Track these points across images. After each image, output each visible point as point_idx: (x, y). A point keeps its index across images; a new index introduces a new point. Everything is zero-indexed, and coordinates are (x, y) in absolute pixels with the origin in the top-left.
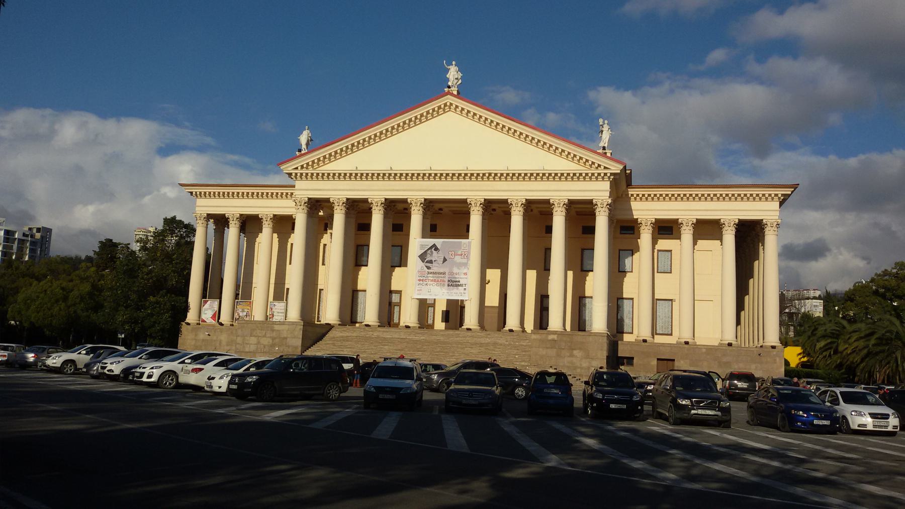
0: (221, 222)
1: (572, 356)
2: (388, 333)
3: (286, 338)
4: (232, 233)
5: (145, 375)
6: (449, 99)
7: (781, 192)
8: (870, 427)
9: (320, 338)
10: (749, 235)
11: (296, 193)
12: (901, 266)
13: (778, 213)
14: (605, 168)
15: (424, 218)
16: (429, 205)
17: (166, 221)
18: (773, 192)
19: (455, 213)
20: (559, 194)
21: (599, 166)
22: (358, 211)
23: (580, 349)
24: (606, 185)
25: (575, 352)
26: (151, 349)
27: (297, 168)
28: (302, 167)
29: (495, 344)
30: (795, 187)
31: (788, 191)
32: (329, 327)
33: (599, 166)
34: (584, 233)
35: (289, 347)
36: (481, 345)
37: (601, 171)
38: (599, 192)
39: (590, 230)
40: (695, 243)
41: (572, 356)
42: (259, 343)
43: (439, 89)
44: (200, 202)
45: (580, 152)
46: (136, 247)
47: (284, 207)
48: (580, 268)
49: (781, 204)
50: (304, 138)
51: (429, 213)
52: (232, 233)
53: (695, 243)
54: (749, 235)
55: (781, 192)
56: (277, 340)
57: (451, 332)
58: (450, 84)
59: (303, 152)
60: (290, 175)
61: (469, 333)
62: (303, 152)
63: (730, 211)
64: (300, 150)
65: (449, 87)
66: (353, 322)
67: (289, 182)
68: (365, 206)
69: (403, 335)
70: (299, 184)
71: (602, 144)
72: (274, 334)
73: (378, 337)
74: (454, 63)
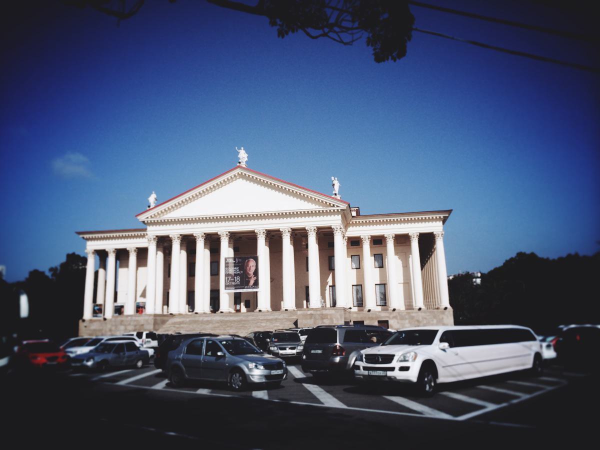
0: (102, 255)
2: (277, 315)
3: (143, 325)
5: (395, 364)
6: (238, 171)
10: (427, 242)
11: (148, 233)
13: (442, 228)
14: (337, 206)
17: (69, 256)
20: (311, 224)
21: (334, 205)
22: (189, 243)
23: (327, 318)
24: (339, 217)
26: (289, 347)
27: (148, 218)
29: (276, 319)
30: (450, 212)
33: (334, 205)
36: (268, 320)
37: (335, 208)
39: (331, 245)
40: (137, 269)
42: (126, 329)
43: (236, 165)
44: (89, 243)
45: (322, 198)
46: (48, 274)
47: (141, 243)
48: (328, 268)
49: (444, 222)
50: (152, 199)
51: (232, 240)
53: (137, 269)
54: (427, 242)
57: (249, 313)
58: (240, 161)
59: (151, 207)
60: (144, 222)
61: (260, 313)
62: (151, 207)
63: (414, 229)
64: (149, 207)
65: (240, 163)
67: (143, 226)
69: (286, 315)
70: (149, 228)
71: (334, 192)
72: (135, 323)
73: (202, 321)
74: (242, 148)
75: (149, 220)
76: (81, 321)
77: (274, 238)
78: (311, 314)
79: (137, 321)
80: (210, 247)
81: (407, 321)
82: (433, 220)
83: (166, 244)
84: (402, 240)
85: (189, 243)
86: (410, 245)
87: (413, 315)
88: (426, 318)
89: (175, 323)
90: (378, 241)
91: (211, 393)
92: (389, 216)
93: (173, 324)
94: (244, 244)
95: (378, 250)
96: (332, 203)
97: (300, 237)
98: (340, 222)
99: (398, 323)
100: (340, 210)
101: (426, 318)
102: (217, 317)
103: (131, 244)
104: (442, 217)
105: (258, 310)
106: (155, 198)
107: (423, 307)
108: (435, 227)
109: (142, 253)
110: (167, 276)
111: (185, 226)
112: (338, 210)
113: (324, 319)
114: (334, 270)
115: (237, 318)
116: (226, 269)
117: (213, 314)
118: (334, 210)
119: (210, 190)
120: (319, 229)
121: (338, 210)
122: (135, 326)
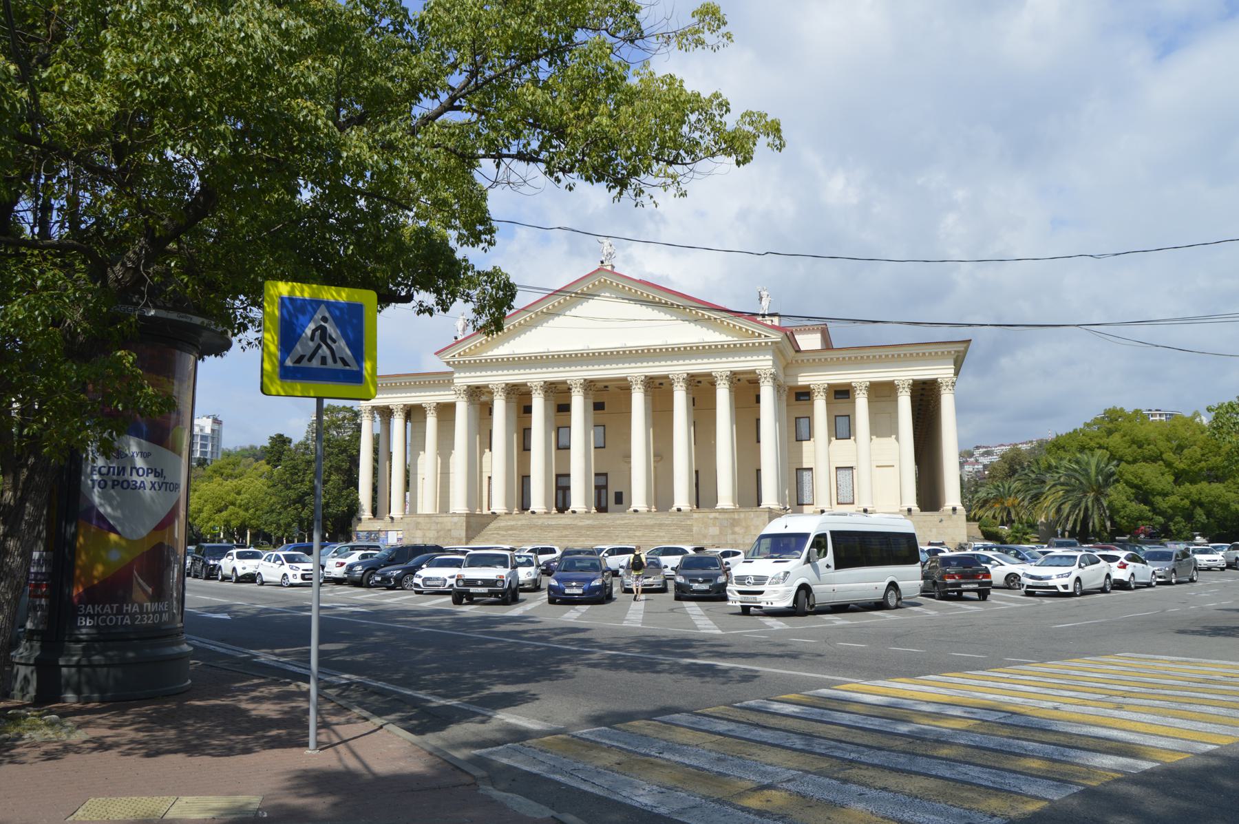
0: (386, 413)
4: (398, 422)
7: (953, 348)
8: (274, 715)
9: (483, 526)
12: (1226, 415)
15: (507, 402)
16: (590, 386)
18: (946, 348)
19: (750, 382)
22: (520, 397)
25: (737, 529)
29: (660, 525)
31: (961, 348)
32: (494, 515)
34: (797, 399)
36: (647, 526)
38: (763, 364)
39: (528, 410)
41: (734, 533)
42: (424, 536)
47: (445, 397)
52: (398, 422)
55: (953, 348)
56: (442, 533)
61: (636, 515)
62: (460, 338)
63: (904, 375)
66: (447, 512)
68: (523, 389)
75: (457, 359)
76: (355, 519)
77: (658, 389)
80: (518, 404)
83: (484, 398)
84: (882, 393)
85: (520, 397)
86: (895, 401)
89: (499, 528)
90: (841, 393)
93: (496, 529)
94: (607, 401)
95: (842, 407)
97: (701, 388)
98: (771, 363)
102: (565, 519)
103: (428, 398)
105: (675, 509)
106: (281, 441)
108: (942, 372)
109: (446, 411)
115: (650, 515)
117: (561, 515)
120: (734, 373)
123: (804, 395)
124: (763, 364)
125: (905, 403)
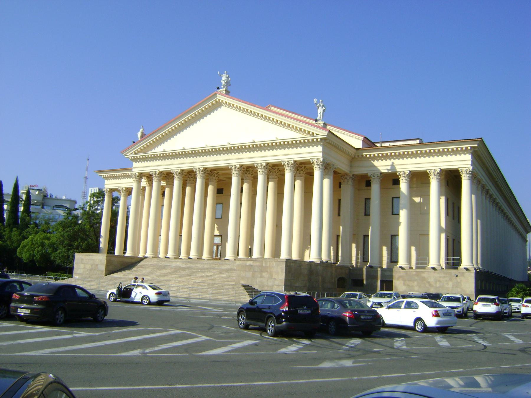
1: (262, 277)
3: (97, 265)
14: (317, 135)
23: (267, 271)
25: (264, 274)
28: (135, 152)
33: (313, 133)
35: (99, 270)
37: (315, 137)
41: (262, 277)
78: (251, 265)
79: (93, 260)
81: (416, 283)
82: (359, 139)
87: (425, 275)
88: (439, 281)
91: (354, 363)
92: (428, 145)
94: (219, 180)
96: (315, 132)
98: (470, 162)
99: (404, 284)
100: (319, 140)
101: (439, 281)
104: (469, 148)
107: (444, 267)
110: (338, 186)
111: (244, 155)
112: (317, 139)
113: (264, 272)
114: (112, 212)
116: (220, 207)
118: (313, 140)
119: (243, 110)
121: (317, 139)
122: (92, 265)
123: (366, 181)
124: (315, 154)
125: (434, 185)
